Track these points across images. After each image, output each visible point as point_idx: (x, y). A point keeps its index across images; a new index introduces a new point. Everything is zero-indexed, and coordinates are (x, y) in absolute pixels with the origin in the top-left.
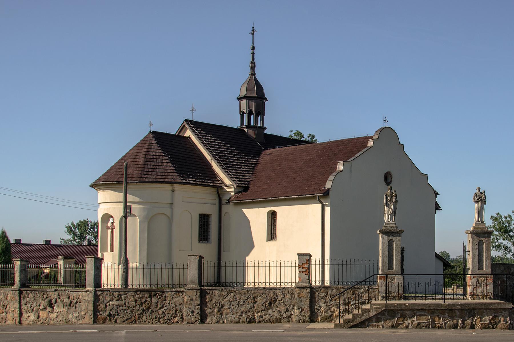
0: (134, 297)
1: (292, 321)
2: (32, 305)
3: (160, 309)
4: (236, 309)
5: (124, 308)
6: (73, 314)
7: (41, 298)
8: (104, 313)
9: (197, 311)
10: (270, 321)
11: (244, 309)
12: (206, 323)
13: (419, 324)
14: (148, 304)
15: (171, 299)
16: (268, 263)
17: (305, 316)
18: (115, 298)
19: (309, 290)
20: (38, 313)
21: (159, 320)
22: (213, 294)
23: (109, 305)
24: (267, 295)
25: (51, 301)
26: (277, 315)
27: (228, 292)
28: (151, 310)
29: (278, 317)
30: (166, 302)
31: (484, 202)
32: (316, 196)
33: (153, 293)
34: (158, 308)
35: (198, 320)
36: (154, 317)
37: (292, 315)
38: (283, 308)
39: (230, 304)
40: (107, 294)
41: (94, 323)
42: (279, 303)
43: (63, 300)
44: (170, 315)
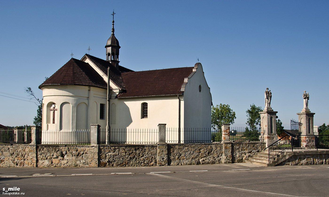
0: (124, 150)
1: (222, 163)
2: (46, 155)
3: (141, 157)
4: (189, 156)
5: (118, 157)
6: (80, 161)
7: (54, 151)
8: (104, 160)
9: (165, 158)
10: (208, 163)
11: (193, 156)
12: (171, 165)
13: (307, 162)
14: (134, 154)
15: (149, 151)
16: (121, 130)
17: (229, 160)
18: (112, 151)
19: (231, 144)
20: (51, 160)
21: (141, 164)
22: (175, 148)
23: (108, 155)
24: (207, 148)
25: (62, 152)
26: (212, 159)
27: (184, 147)
28: (136, 158)
29: (213, 160)
30: (145, 153)
31: (308, 98)
32: (177, 95)
33: (137, 148)
34: (140, 157)
35: (167, 164)
36: (138, 162)
37: (221, 159)
38: (216, 155)
39: (185, 154)
40: (107, 148)
41: (98, 167)
42: (214, 153)
43: (71, 152)
44: (148, 161)
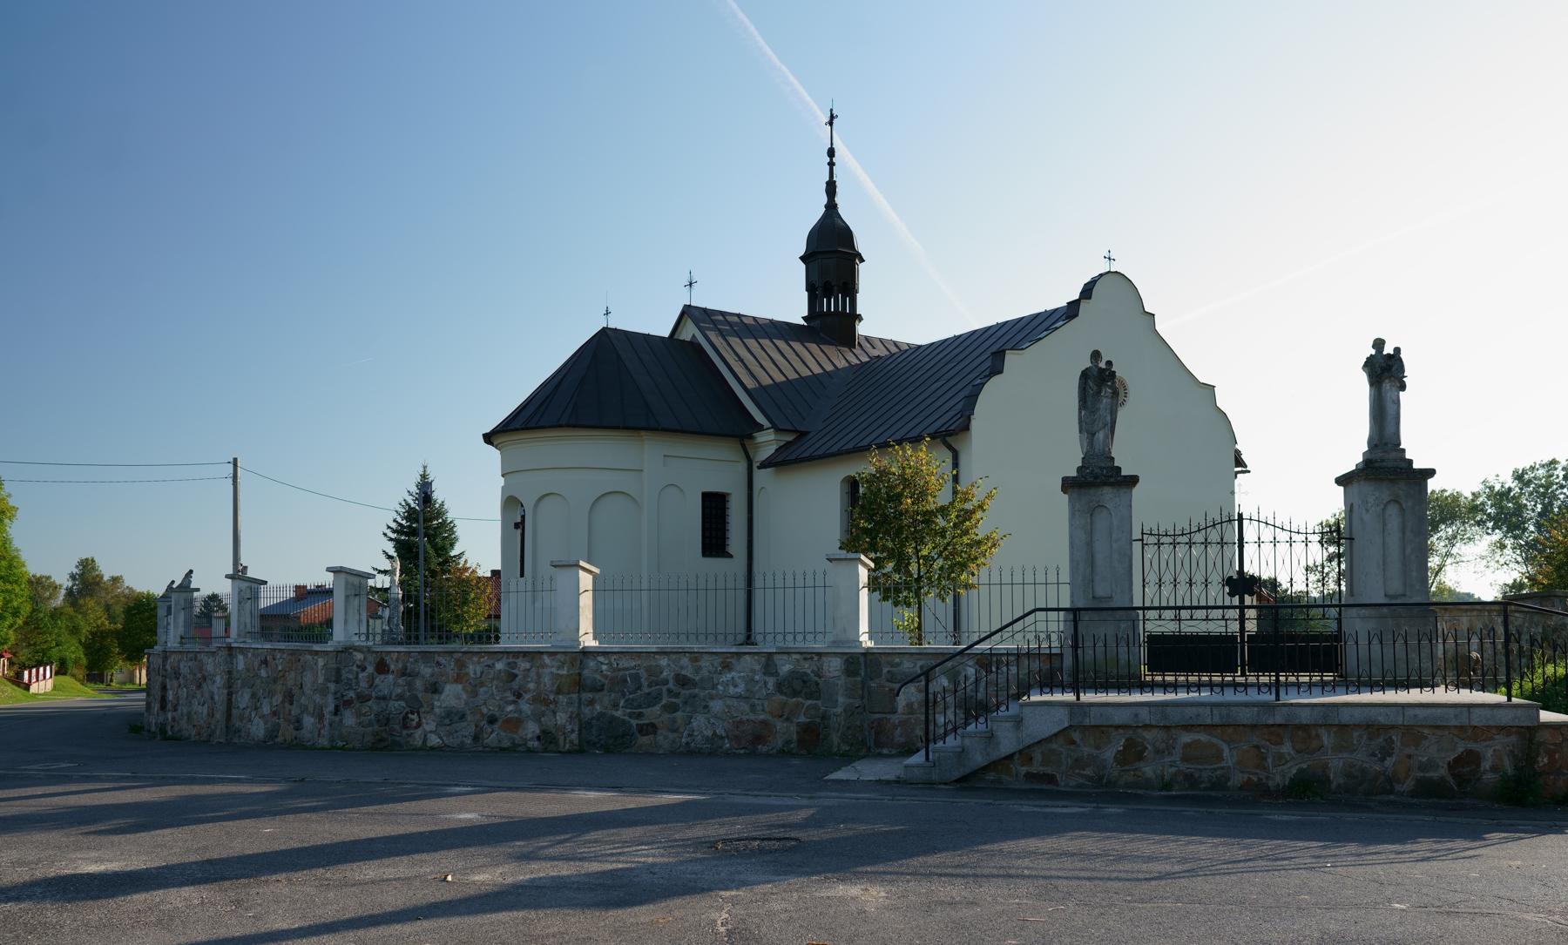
16: (800, 579)
